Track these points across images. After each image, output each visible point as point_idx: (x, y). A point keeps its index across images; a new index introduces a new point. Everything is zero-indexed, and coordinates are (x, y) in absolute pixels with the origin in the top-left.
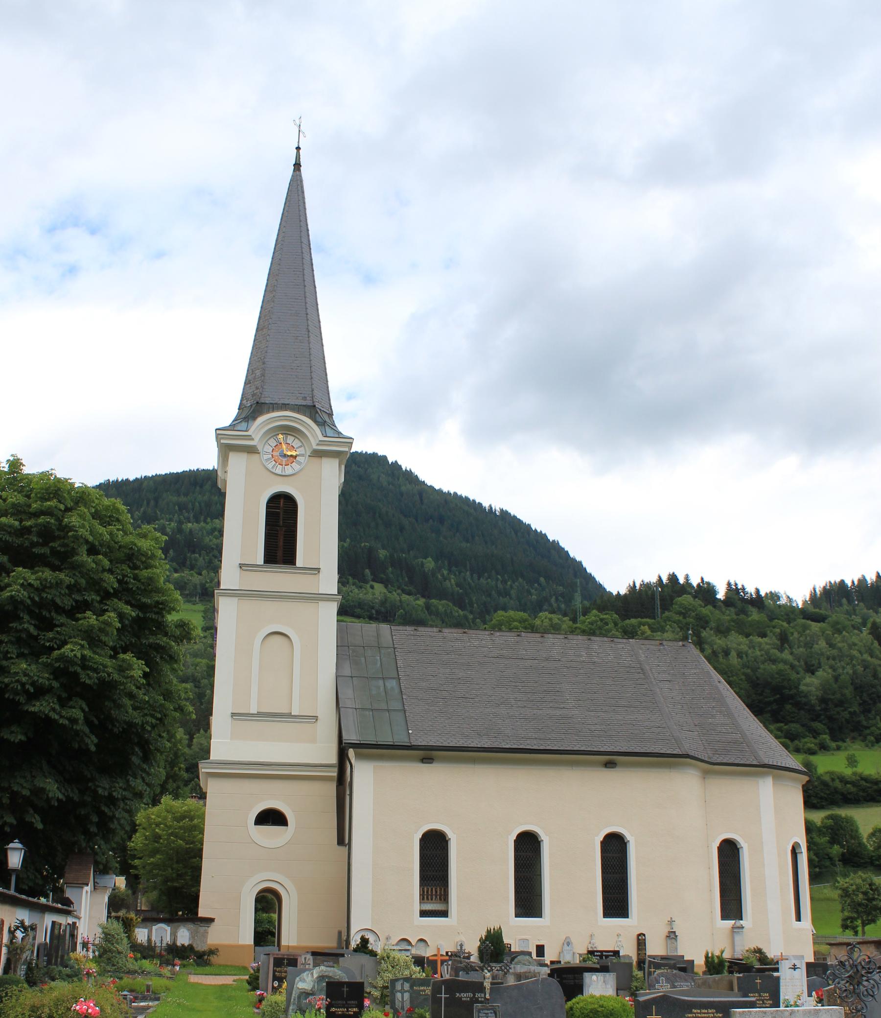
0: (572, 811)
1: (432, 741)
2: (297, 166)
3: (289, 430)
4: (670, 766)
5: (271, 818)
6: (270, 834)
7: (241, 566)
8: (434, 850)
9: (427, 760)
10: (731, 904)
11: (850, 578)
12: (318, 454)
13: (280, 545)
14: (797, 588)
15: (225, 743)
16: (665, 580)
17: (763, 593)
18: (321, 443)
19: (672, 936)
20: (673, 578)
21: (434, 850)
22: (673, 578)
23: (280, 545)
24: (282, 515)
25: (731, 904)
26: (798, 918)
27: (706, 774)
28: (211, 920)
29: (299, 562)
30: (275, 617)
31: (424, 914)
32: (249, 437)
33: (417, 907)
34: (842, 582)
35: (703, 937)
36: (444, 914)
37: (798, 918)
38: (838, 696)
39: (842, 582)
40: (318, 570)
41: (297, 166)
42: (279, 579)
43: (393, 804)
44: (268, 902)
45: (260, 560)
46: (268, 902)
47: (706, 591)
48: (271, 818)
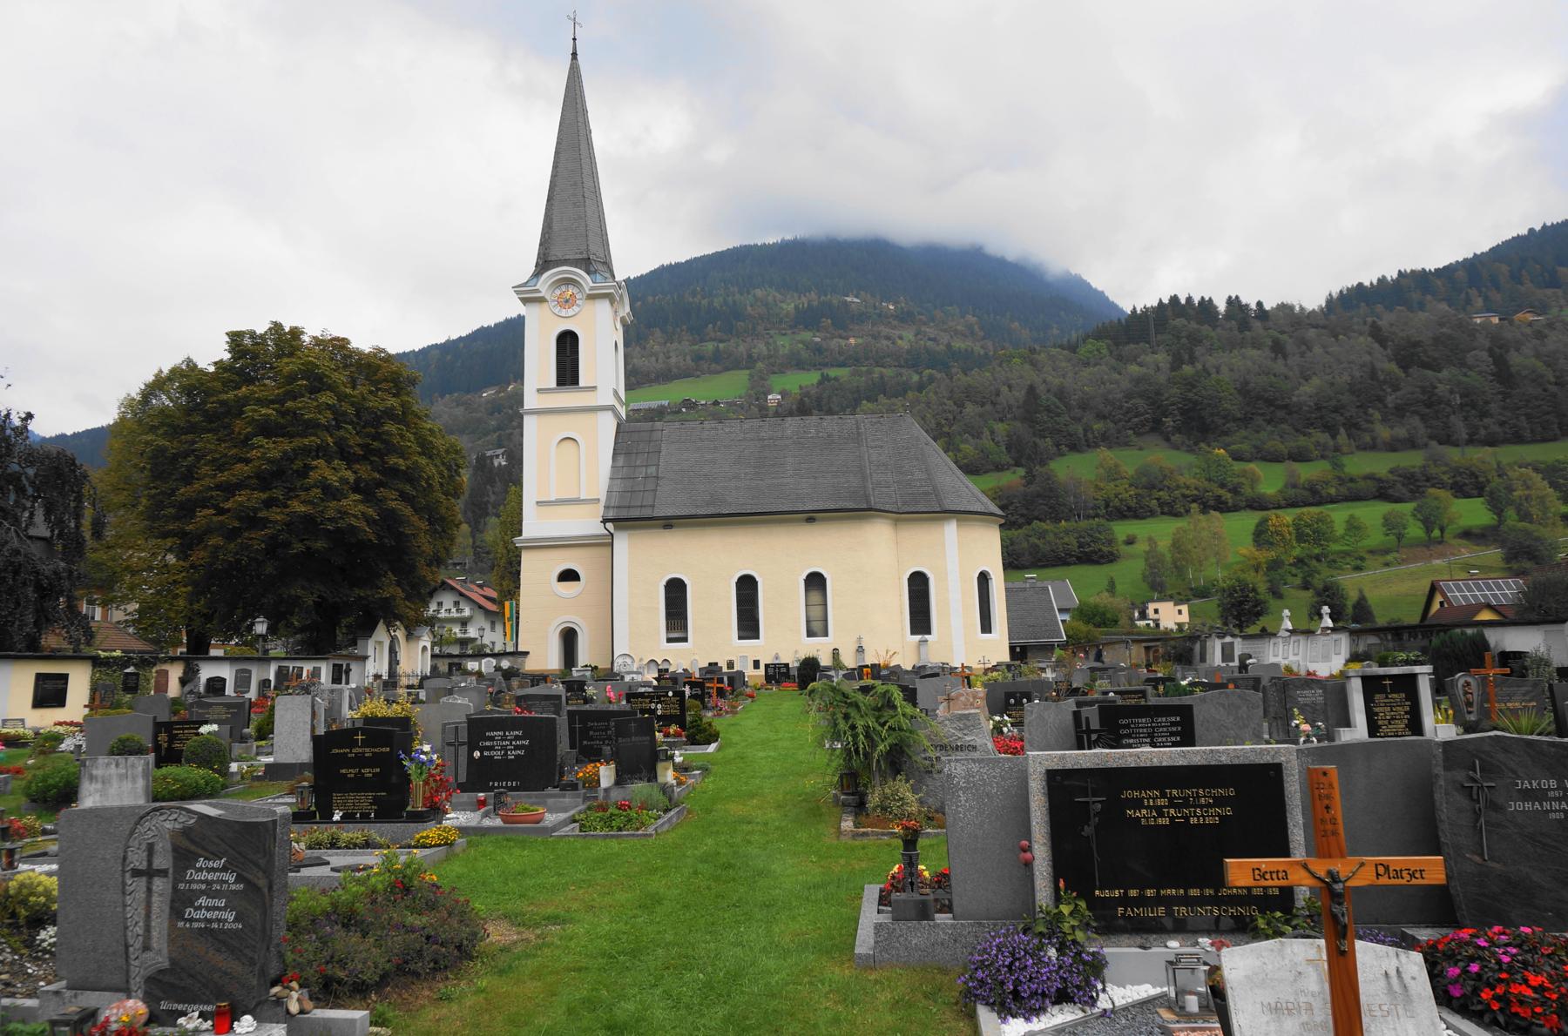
0: (778, 560)
1: (670, 512)
2: (574, 55)
3: (569, 282)
4: (860, 518)
5: (569, 576)
6: (569, 588)
7: (539, 390)
8: (676, 592)
9: (668, 526)
10: (920, 620)
11: (1369, 278)
12: (591, 297)
13: (568, 373)
14: (1311, 296)
15: (534, 524)
16: (1166, 301)
17: (1267, 307)
18: (592, 288)
19: (860, 650)
20: (1174, 299)
21: (676, 592)
22: (1174, 299)
23: (568, 373)
24: (567, 344)
25: (920, 620)
26: (986, 627)
27: (896, 522)
28: (527, 653)
29: (582, 383)
30: (567, 426)
31: (669, 640)
32: (538, 291)
33: (663, 635)
34: (1360, 285)
35: (894, 645)
36: (685, 640)
37: (986, 627)
38: (1334, 403)
39: (1360, 285)
40: (595, 388)
41: (574, 55)
42: (568, 398)
43: (643, 564)
44: (569, 638)
45: (553, 384)
46: (569, 638)
47: (1207, 305)
48: (569, 576)
